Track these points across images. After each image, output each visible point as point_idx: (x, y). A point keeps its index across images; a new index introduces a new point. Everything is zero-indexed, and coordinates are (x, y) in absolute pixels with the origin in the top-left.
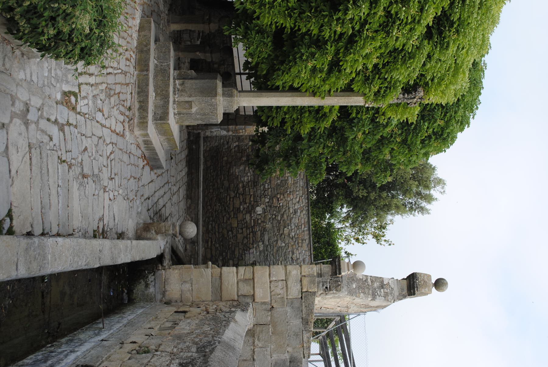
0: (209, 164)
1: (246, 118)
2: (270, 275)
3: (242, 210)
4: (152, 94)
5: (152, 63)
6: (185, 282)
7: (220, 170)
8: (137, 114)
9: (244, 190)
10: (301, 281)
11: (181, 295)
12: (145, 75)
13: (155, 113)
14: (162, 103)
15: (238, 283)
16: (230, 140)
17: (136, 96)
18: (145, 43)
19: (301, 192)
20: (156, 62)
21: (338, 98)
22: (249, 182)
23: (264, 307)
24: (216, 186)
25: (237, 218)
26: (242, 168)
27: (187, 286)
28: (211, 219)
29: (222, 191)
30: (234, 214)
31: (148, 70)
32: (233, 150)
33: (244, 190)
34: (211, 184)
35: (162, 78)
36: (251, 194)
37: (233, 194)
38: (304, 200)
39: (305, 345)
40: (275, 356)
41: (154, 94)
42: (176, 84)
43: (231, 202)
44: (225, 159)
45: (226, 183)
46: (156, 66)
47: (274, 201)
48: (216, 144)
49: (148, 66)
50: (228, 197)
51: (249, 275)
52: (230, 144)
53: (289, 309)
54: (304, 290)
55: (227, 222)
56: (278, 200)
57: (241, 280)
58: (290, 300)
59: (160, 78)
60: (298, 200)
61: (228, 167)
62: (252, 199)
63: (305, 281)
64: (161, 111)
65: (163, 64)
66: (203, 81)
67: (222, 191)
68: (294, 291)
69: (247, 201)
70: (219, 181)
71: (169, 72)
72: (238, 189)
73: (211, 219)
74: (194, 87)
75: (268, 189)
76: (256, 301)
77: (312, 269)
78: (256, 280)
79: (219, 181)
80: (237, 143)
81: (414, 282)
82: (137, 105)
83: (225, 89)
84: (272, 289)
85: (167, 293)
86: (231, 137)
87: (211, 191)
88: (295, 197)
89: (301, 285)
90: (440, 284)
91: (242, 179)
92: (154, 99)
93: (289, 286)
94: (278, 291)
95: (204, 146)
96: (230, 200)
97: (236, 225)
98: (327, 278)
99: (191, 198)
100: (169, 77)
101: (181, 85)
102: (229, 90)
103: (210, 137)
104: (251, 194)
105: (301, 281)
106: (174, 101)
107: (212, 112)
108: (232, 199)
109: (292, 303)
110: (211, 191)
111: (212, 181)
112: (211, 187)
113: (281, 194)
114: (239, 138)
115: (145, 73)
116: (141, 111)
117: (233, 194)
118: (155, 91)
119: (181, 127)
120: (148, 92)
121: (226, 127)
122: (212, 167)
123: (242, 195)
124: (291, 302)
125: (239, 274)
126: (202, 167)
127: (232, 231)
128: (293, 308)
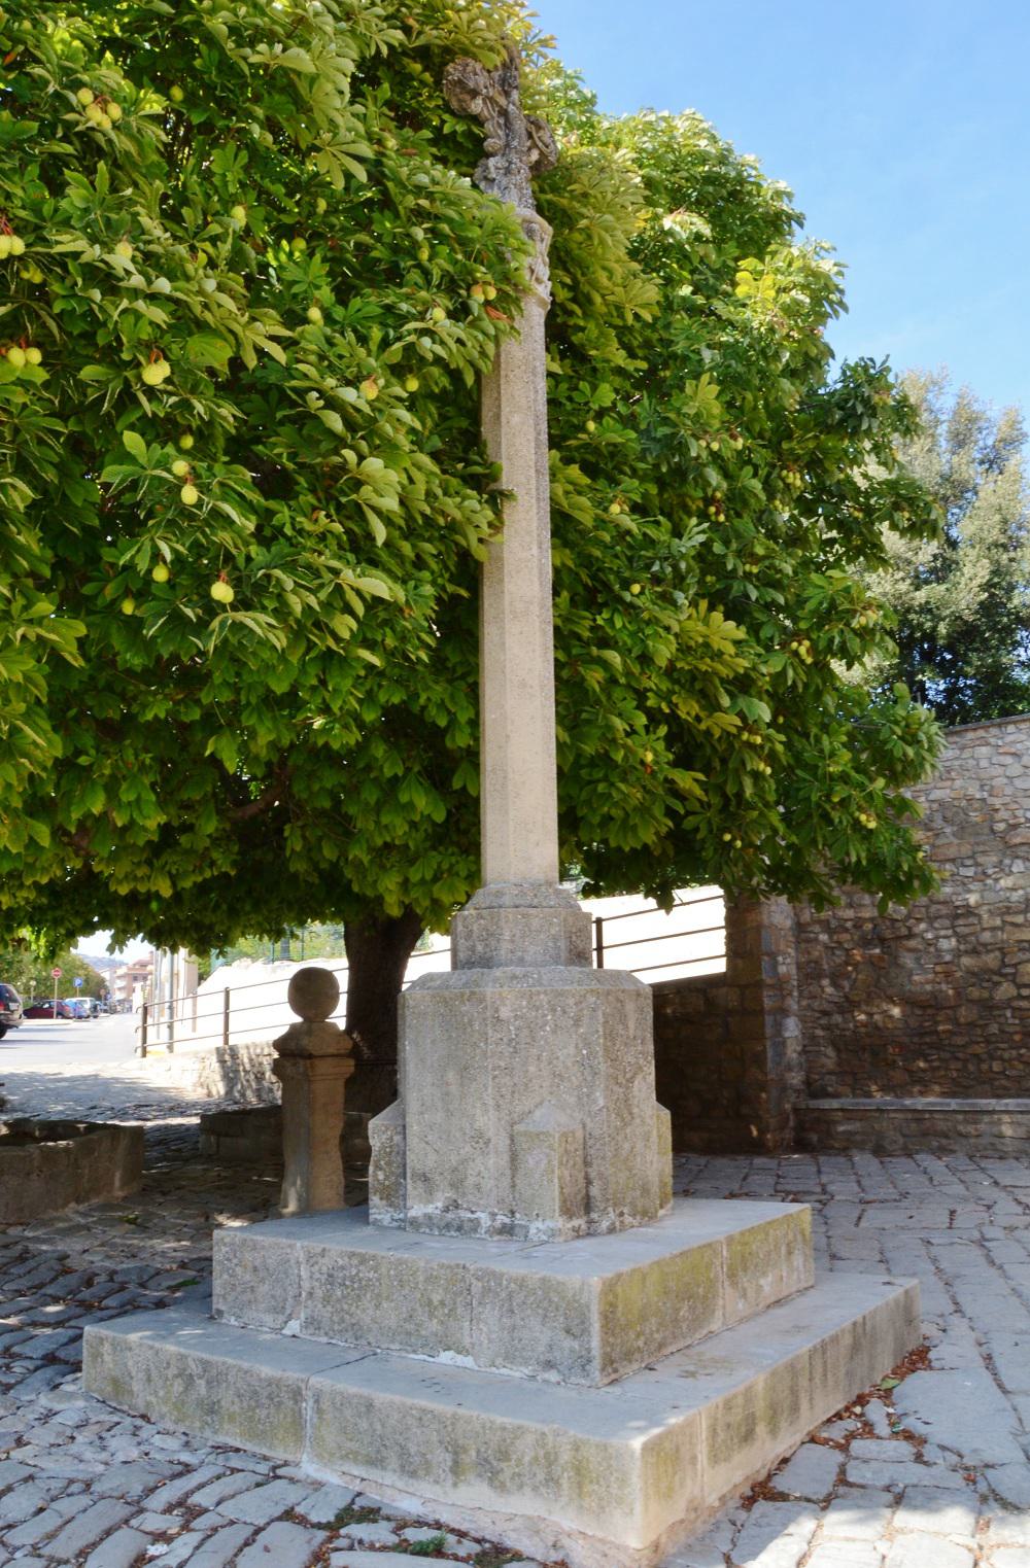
12: (319, 1411)
16: (816, 1004)
19: (984, 750)
21: (505, 410)
22: (956, 934)
29: (994, 1028)
34: (971, 1067)
35: (367, 1301)
36: (998, 922)
38: (1011, 738)
42: (429, 1217)
47: (1018, 840)
50: (1016, 1004)
52: (826, 1006)
56: (1015, 827)
60: (1009, 760)
65: (306, 1285)
67: (994, 1028)
70: (960, 1041)
74: (439, 1117)
75: (977, 864)
79: (960, 1041)
80: (825, 982)
86: (804, 1003)
88: (1000, 770)
91: (948, 958)
103: (809, 1072)
104: (998, 922)
107: (577, 1022)
110: (996, 1066)
112: (985, 1067)
113: (993, 821)
114: (807, 976)
116: (508, 1470)
117: (1006, 990)
119: (686, 1186)
121: (769, 1020)
123: (1004, 955)
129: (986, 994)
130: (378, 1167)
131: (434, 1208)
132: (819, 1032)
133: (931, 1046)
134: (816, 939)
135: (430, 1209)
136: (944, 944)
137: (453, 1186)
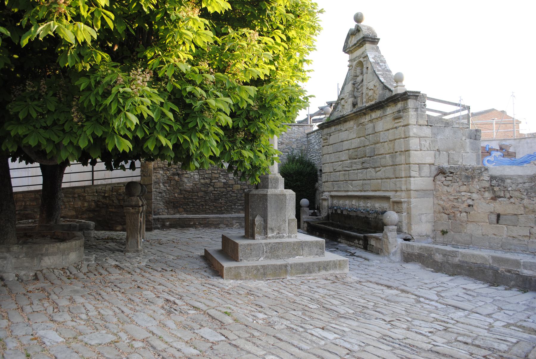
0: (181, 210)
1: (144, 175)
2: (416, 150)
3: (225, 181)
4: (298, 259)
5: (262, 261)
6: (420, 220)
7: (188, 199)
8: (331, 272)
9: (207, 178)
10: (420, 125)
11: (429, 222)
12: (291, 268)
13: (317, 254)
14: (306, 249)
15: (421, 177)
16: (158, 190)
17: (314, 274)
18: (255, 272)
20: (262, 258)
23: (437, 156)
24: (203, 203)
25: (232, 185)
26: (186, 180)
27: (424, 218)
28: (233, 206)
30: (229, 187)
31: (286, 266)
32: (168, 188)
33: (207, 178)
34: (201, 207)
35: (280, 251)
36: (210, 172)
37: (211, 188)
39: (461, 127)
40: (468, 150)
41: (297, 257)
42: (273, 236)
43: (219, 189)
44: (176, 195)
45: (200, 194)
46: (267, 257)
48: (161, 203)
49: (281, 265)
51: (416, 167)
52: (161, 191)
53: (439, 137)
54: (426, 123)
55: (236, 193)
57: (420, 174)
58: (433, 136)
59: (280, 253)
61: (185, 193)
62: (216, 172)
63: (421, 122)
64: (315, 248)
65: (265, 250)
66: (269, 208)
67: (208, 198)
68: (427, 131)
69: (217, 176)
70: (198, 201)
71: (274, 243)
72: (206, 183)
73: (233, 206)
74: (275, 217)
76: (433, 162)
77: (412, 115)
78: (420, 162)
79: (198, 201)
80: (161, 184)
81: (371, 38)
82: (323, 272)
83: (270, 186)
84: (425, 149)
85: (428, 234)
87: (207, 207)
89: (423, 125)
90: (358, 19)
92: (302, 257)
93: (424, 135)
94: (427, 144)
95: (163, 215)
96: (217, 191)
97: (239, 186)
98: (418, 104)
99: (218, 224)
100: (279, 243)
101: (272, 230)
102: (271, 182)
104: (210, 172)
105: (420, 125)
106: (289, 237)
108: (216, 189)
109: (435, 134)
110: (207, 207)
111: (198, 207)
112: (204, 207)
115: (289, 268)
117: (211, 188)
118: (294, 256)
120: (309, 263)
122: (185, 207)
123: (211, 180)
124: (434, 135)
125: (416, 176)
126: (185, 216)
127: (244, 189)
128: (438, 134)
129: (206, 189)
130: (257, 228)
131: (274, 234)
132: (158, 198)
133: (190, 202)
134: (159, 173)
135: (273, 235)
136: (196, 176)
137: (278, 230)
